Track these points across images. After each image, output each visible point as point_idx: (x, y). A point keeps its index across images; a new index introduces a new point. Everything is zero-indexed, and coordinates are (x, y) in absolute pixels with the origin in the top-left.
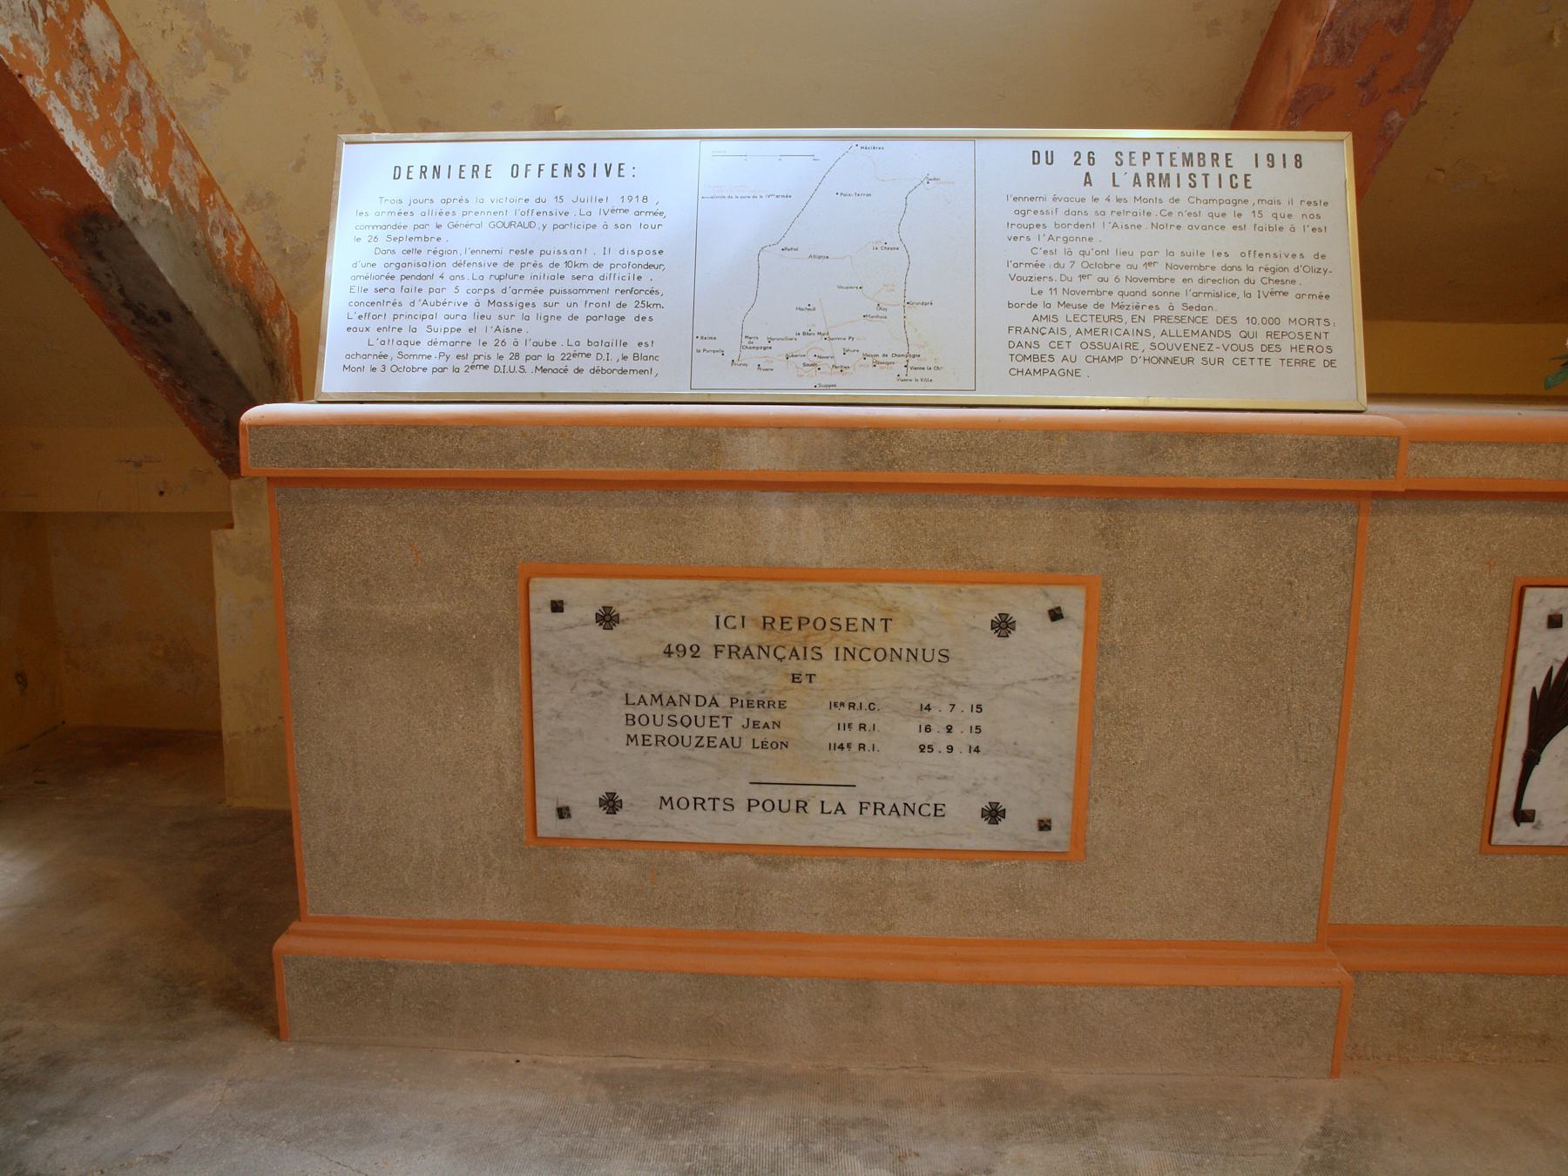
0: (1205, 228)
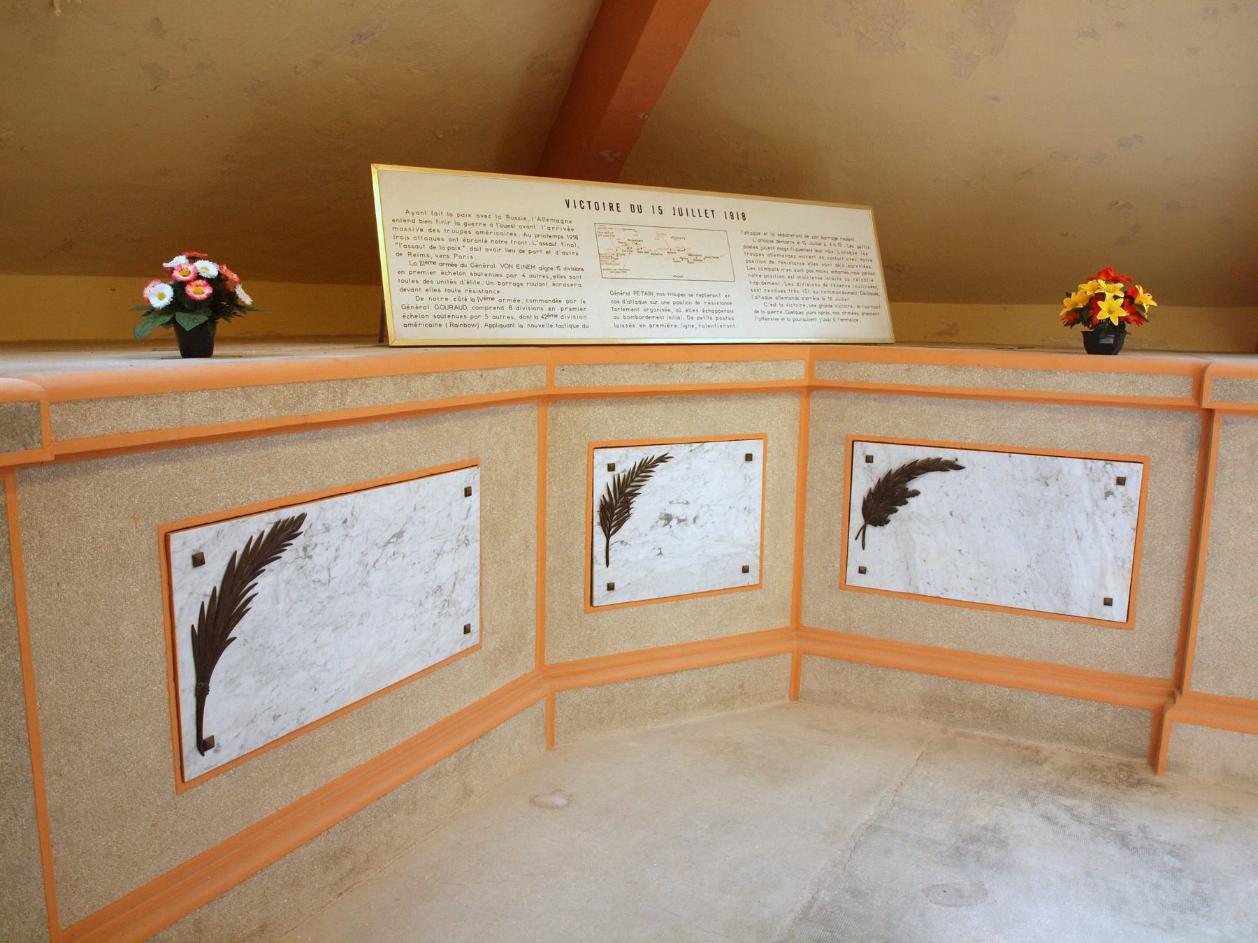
0: (431, 325)
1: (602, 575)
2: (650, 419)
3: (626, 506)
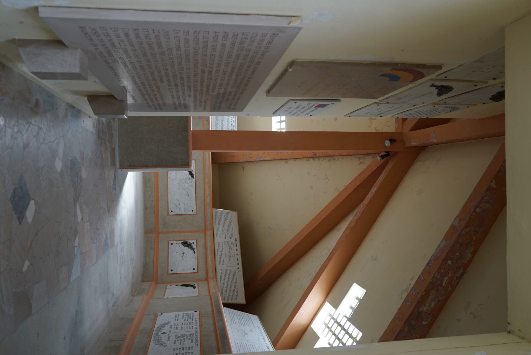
1: (174, 243)
2: (202, 250)
3: (187, 246)
